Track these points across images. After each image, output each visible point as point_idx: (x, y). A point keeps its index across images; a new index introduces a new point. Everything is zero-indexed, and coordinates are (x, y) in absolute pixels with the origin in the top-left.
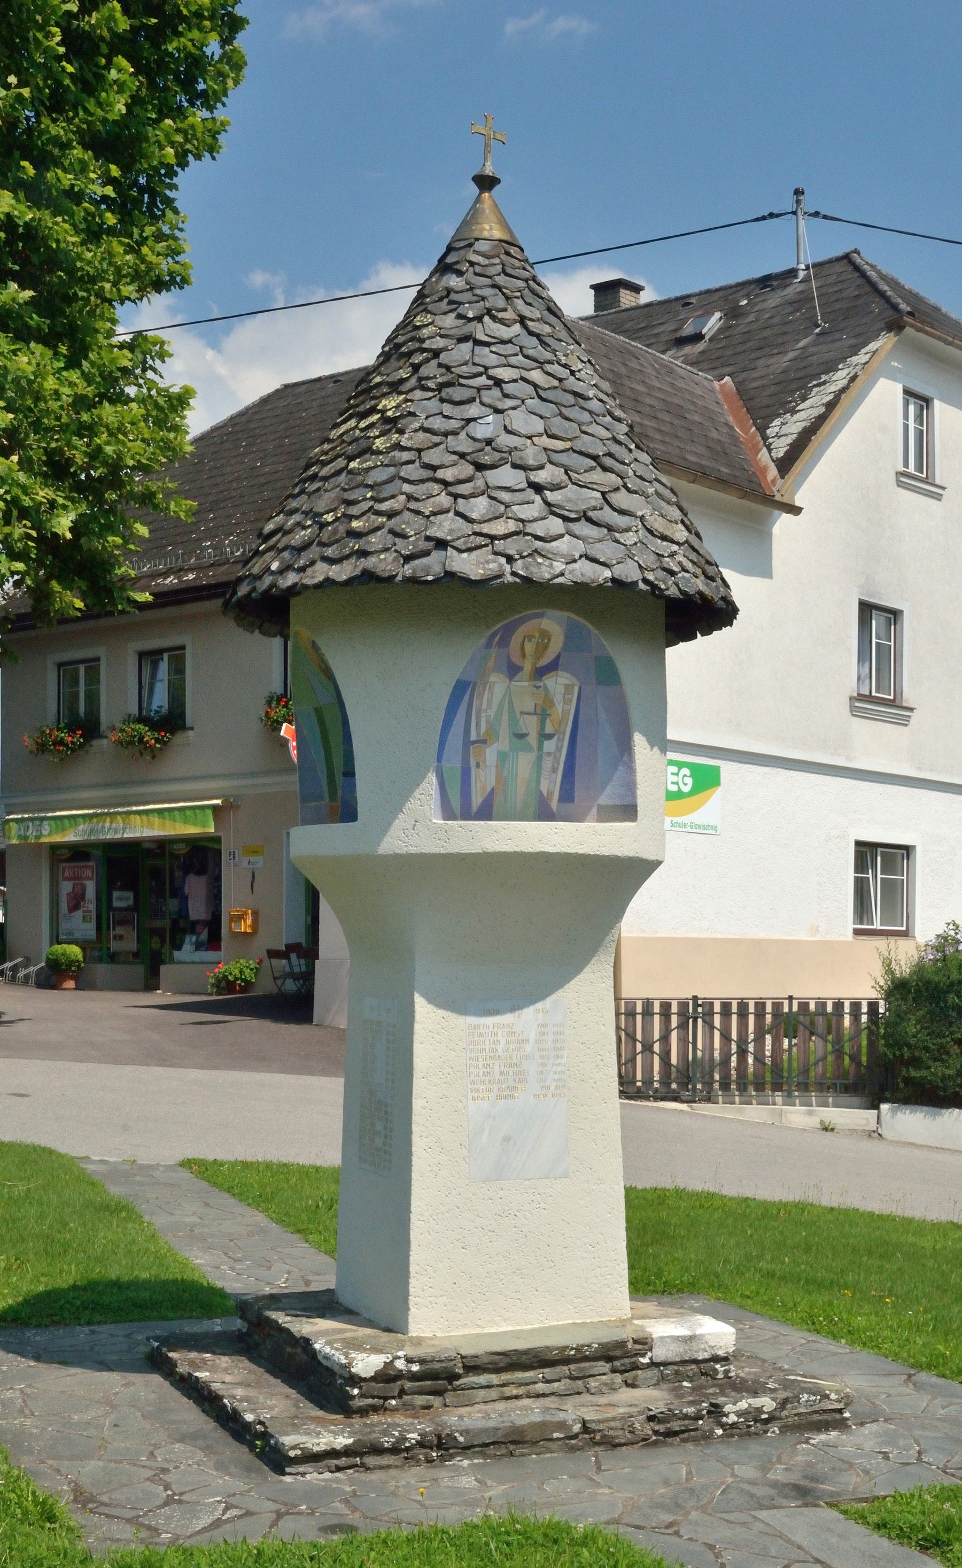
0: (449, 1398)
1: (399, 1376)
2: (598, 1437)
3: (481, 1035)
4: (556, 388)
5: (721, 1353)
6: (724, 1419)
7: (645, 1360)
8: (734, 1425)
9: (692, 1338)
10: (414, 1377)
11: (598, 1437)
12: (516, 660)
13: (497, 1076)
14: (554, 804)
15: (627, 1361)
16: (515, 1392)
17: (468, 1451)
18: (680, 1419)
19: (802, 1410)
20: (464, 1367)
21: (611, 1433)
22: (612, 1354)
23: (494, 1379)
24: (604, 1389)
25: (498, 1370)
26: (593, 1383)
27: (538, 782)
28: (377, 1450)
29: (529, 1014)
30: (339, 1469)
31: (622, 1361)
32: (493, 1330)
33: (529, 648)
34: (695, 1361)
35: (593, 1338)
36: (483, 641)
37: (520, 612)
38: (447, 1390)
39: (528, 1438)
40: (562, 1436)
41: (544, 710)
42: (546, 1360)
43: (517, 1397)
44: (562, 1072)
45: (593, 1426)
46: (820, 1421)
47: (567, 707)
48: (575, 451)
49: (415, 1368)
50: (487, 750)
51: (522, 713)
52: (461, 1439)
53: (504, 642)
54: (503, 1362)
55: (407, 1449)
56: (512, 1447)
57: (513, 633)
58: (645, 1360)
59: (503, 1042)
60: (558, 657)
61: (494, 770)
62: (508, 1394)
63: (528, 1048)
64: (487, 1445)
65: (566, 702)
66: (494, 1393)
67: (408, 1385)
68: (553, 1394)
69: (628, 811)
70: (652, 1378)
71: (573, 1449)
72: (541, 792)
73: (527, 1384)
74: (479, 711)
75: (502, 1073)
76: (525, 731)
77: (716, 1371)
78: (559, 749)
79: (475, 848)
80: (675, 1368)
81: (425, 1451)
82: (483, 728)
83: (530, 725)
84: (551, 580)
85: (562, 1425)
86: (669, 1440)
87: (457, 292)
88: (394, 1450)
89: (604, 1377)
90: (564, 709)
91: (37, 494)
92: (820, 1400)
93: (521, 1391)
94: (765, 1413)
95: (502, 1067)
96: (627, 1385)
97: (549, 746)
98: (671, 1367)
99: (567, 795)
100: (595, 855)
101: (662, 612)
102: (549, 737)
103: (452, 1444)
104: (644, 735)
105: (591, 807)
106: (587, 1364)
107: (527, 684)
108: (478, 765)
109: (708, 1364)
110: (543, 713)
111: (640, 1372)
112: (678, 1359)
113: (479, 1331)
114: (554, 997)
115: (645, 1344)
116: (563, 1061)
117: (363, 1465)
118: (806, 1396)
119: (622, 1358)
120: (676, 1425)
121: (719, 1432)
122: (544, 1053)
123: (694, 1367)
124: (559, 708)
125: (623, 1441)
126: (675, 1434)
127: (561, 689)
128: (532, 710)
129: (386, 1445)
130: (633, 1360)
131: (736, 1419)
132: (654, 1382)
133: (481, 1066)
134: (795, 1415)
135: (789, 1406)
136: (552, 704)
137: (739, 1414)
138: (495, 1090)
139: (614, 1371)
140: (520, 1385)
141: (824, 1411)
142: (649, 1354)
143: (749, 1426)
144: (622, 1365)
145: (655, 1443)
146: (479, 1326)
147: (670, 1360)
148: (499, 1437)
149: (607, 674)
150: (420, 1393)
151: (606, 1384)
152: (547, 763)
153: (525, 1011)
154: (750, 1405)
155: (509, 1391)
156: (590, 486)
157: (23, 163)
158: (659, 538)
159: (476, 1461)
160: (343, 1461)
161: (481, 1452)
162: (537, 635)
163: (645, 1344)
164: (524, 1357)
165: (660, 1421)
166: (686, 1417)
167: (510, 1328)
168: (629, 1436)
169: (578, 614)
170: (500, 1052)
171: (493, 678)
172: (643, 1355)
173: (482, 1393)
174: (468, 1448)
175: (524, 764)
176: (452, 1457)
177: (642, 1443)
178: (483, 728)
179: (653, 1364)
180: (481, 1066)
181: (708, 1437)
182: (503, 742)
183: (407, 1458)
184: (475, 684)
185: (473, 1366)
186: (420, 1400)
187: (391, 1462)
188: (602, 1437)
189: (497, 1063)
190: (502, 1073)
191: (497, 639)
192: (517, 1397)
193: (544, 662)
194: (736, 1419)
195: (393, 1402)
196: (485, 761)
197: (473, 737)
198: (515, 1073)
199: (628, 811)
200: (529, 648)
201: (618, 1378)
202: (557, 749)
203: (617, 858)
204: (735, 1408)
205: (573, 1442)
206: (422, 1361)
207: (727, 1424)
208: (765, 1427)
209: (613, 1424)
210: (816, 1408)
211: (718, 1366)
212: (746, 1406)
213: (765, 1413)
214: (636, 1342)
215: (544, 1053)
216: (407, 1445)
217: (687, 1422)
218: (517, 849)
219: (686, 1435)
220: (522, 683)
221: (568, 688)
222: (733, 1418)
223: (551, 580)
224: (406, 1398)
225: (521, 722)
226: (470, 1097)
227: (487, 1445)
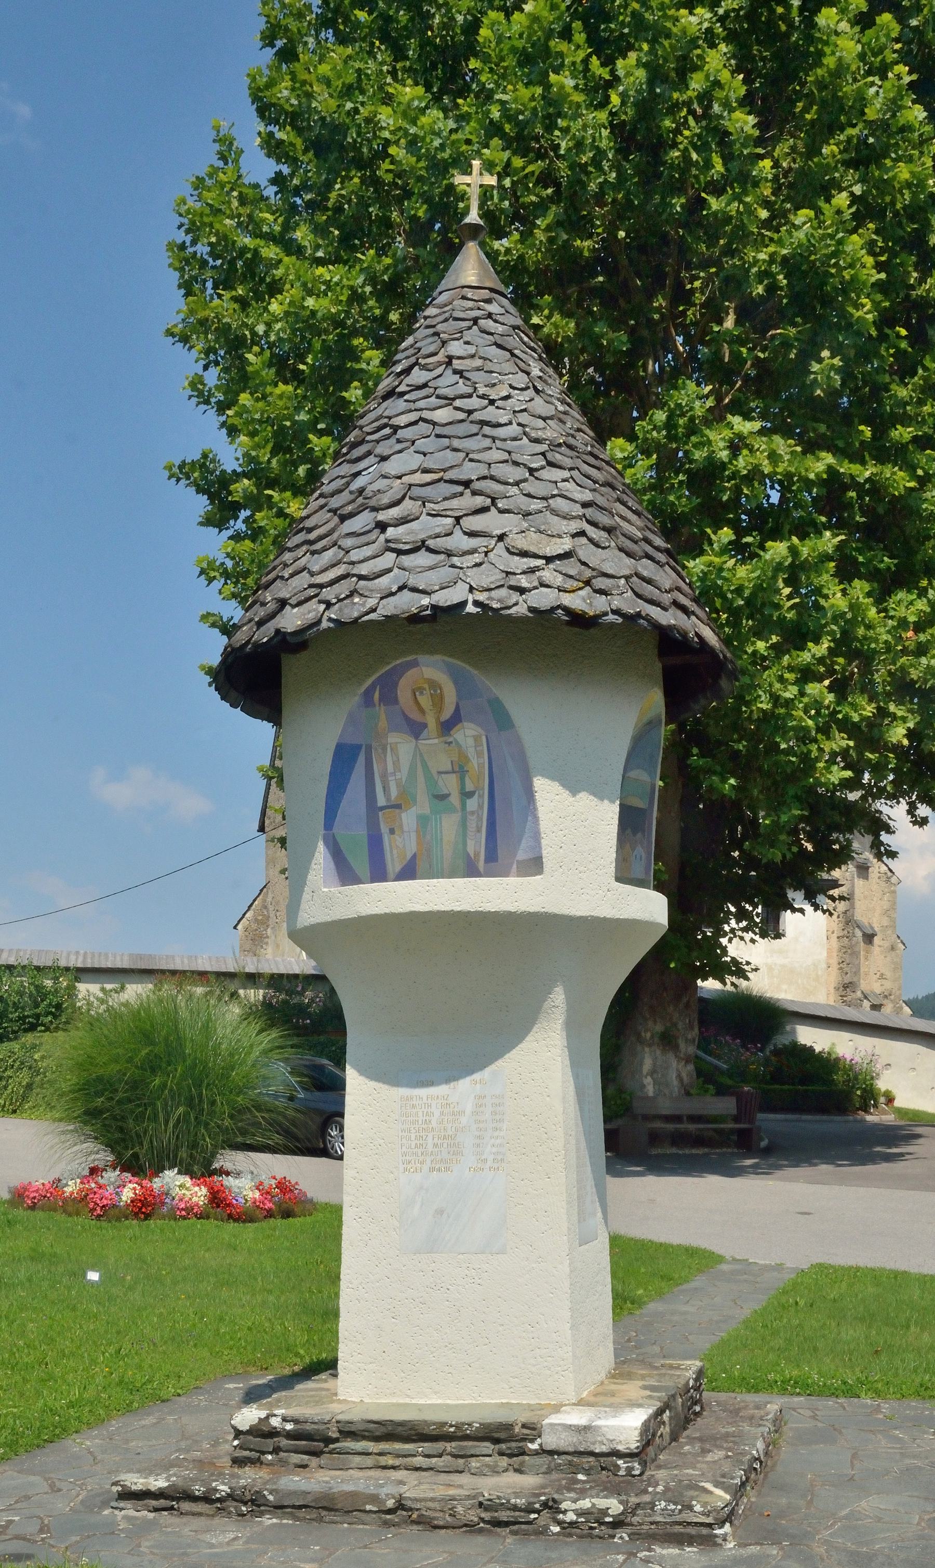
0: (324, 1460)
1: (273, 1433)
2: (414, 1516)
3: (414, 1106)
4: (462, 421)
5: (621, 1448)
6: (561, 1516)
7: (534, 1446)
8: (572, 1524)
9: (586, 1429)
10: (290, 1435)
11: (414, 1516)
12: (415, 715)
13: (430, 1148)
14: (481, 865)
15: (514, 1444)
16: (391, 1461)
17: (279, 1511)
18: (509, 1509)
19: (659, 1519)
20: (340, 1432)
21: (429, 1513)
22: (496, 1435)
23: (371, 1446)
24: (486, 1470)
25: (377, 1439)
26: (474, 1463)
27: (465, 844)
28: (190, 1497)
29: (465, 1085)
30: (156, 1510)
31: (509, 1445)
32: (422, 1402)
33: (425, 701)
34: (592, 1454)
35: (476, 1418)
36: (357, 699)
37: (388, 663)
38: (322, 1452)
39: (339, 1506)
40: (375, 1509)
41: (461, 767)
42: (422, 1434)
43: (394, 1468)
44: (501, 1145)
45: (409, 1504)
46: (682, 1534)
47: (481, 761)
48: (446, 481)
49: (289, 1427)
50: (404, 815)
51: (440, 773)
52: (271, 1498)
53: (390, 698)
54: (380, 1431)
55: (219, 1500)
56: (324, 1513)
57: (396, 685)
58: (534, 1446)
59: (437, 1114)
60: (457, 709)
61: (413, 836)
62: (383, 1464)
63: (464, 1120)
64: (300, 1507)
65: (479, 755)
66: (369, 1461)
67: (284, 1442)
68: (431, 1469)
69: (535, 865)
70: (542, 1466)
71: (386, 1524)
72: (468, 855)
73: (405, 1456)
74: (384, 777)
75: (435, 1145)
76: (446, 792)
77: (618, 1467)
78: (481, 807)
79: (349, 913)
80: (569, 1458)
81: (235, 1504)
82: (394, 792)
83: (450, 784)
84: (360, 617)
85: (374, 1499)
86: (499, 1530)
87: (459, 358)
88: (206, 1499)
89: (487, 1459)
90: (478, 763)
91: (865, 710)
92: (680, 1511)
93: (397, 1462)
94: (609, 1515)
95: (436, 1140)
96: (516, 1470)
97: (472, 804)
98: (564, 1457)
99: (492, 856)
100: (476, 912)
101: (653, 652)
102: (470, 795)
103: (261, 1501)
104: (553, 779)
105: (512, 864)
106: (470, 1443)
107: (436, 741)
108: (392, 831)
109: (610, 1459)
110: (460, 770)
111: (527, 1458)
112: (571, 1449)
113: (407, 1401)
114: (493, 1067)
115: (534, 1429)
116: (502, 1134)
117: (178, 1510)
118: (663, 1503)
119: (510, 1441)
120: (504, 1515)
121: (557, 1529)
122: (481, 1125)
123: (591, 1459)
124: (474, 762)
125: (441, 1523)
126: (507, 1524)
127: (471, 742)
128: (449, 768)
129: (197, 1493)
130: (521, 1444)
131: (575, 1518)
132: (543, 1469)
133: (413, 1138)
134: (652, 1523)
135: (639, 1512)
136: (467, 760)
137: (579, 1513)
138: (429, 1161)
139: (501, 1454)
140: (398, 1456)
141: (689, 1524)
142: (539, 1440)
143: (591, 1528)
144: (509, 1448)
145: (481, 1531)
146: (408, 1396)
147: (562, 1449)
148: (308, 1500)
149: (502, 720)
150: (296, 1452)
151: (487, 1466)
152: (472, 823)
153: (461, 1082)
154: (594, 1505)
155: (384, 1460)
156: (444, 513)
157: (862, 428)
158: (517, 555)
159: (285, 1521)
160: (162, 1503)
161: (291, 1513)
162: (426, 686)
163: (534, 1429)
164: (400, 1428)
165: (487, 1509)
166: (515, 1508)
167: (439, 1401)
168: (449, 1519)
169: (451, 656)
170: (434, 1124)
171: (393, 738)
172: (532, 1441)
173: (357, 1459)
174: (276, 1507)
175: (448, 826)
176: (261, 1514)
177: (464, 1529)
178: (394, 792)
179: (543, 1451)
180: (413, 1138)
181: (541, 1533)
182: (423, 805)
183: (219, 1509)
184: (369, 749)
185: (349, 1432)
186: (296, 1458)
187: (203, 1511)
188: (419, 1516)
189: (430, 1135)
190: (435, 1145)
191: (377, 695)
192: (394, 1468)
193: (447, 714)
194: (575, 1518)
195: (270, 1457)
196: (401, 826)
197: (381, 801)
198: (449, 1145)
199: (535, 865)
200: (425, 701)
201: (504, 1462)
202: (477, 805)
203: (510, 914)
204: (574, 1506)
205: (388, 1517)
206: (296, 1421)
207: (565, 1522)
208: (611, 1531)
209: (430, 1504)
210: (678, 1518)
211: (620, 1462)
212: (589, 1505)
213: (609, 1515)
214: (524, 1426)
215: (481, 1125)
216: (218, 1496)
217: (517, 1513)
218: (387, 911)
219: (516, 1527)
220: (431, 741)
221: (477, 738)
222: (571, 1517)
223: (360, 617)
224: (282, 1454)
225: (440, 783)
226: (401, 1169)
227: (300, 1507)
